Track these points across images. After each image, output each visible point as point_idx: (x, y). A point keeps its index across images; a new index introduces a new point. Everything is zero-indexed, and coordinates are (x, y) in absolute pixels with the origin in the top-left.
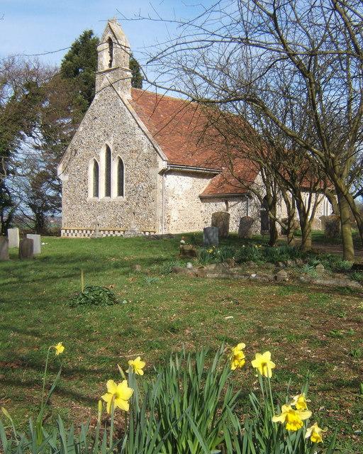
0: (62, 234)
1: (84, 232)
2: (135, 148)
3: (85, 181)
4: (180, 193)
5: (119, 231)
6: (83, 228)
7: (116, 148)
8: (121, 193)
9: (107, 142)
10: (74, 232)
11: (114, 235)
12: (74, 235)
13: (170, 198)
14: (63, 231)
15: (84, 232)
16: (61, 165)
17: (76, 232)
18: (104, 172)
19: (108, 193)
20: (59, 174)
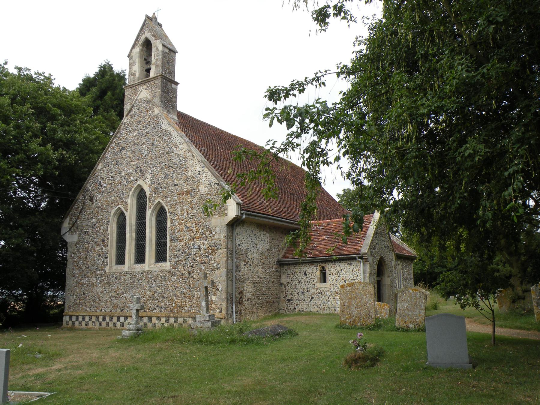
0: (64, 323)
1: (101, 319)
2: (186, 188)
3: (103, 241)
4: (255, 256)
5: (159, 318)
6: (98, 313)
7: (155, 190)
8: (161, 257)
9: (140, 182)
10: (104, 319)
11: (166, 325)
12: (83, 323)
13: (243, 264)
14: (66, 318)
15: (101, 319)
16: (68, 219)
17: (87, 319)
18: (115, 235)
19: (140, 258)
20: (63, 231)
